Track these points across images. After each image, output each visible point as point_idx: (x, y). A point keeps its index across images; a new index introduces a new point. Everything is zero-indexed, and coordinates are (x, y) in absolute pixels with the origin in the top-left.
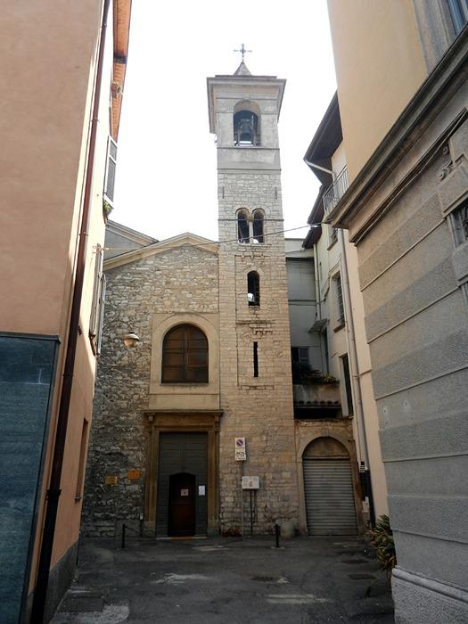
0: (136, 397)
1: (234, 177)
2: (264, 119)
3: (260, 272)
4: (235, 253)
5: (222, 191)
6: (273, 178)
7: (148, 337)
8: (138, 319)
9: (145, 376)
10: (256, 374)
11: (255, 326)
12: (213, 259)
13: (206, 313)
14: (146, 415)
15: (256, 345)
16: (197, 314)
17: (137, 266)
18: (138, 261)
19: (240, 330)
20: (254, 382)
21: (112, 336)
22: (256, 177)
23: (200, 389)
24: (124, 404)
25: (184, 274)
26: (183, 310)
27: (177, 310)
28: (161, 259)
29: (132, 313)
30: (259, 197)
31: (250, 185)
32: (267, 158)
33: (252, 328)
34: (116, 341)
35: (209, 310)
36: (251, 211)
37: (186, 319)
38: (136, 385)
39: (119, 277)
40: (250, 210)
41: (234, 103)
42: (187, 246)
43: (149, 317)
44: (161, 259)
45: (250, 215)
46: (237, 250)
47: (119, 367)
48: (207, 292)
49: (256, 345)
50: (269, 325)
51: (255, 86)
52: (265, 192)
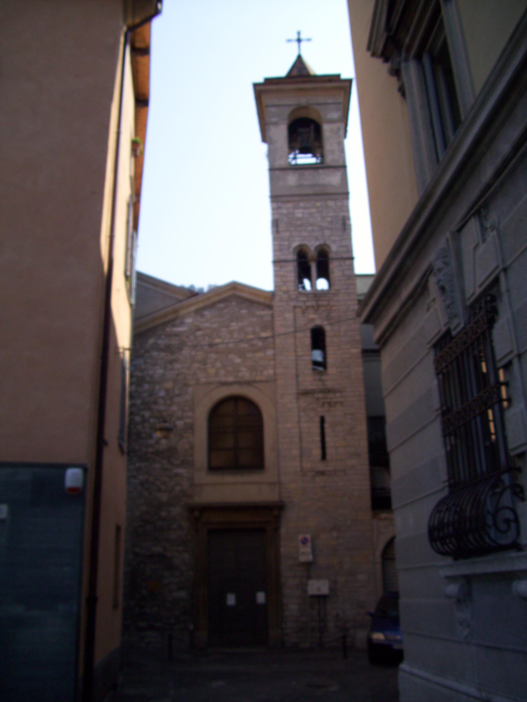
0: (178, 488)
1: (290, 205)
2: (327, 129)
3: (327, 328)
4: (293, 304)
5: (276, 224)
6: (339, 204)
7: (190, 414)
8: (177, 392)
9: (187, 463)
10: (324, 456)
11: (321, 395)
12: (266, 312)
13: (261, 382)
14: (191, 509)
15: (322, 420)
16: (249, 383)
17: (174, 326)
18: (174, 320)
19: (304, 402)
20: (321, 466)
21: (147, 414)
22: (318, 204)
23: (255, 477)
24: (164, 497)
25: (231, 333)
26: (231, 379)
27: (223, 379)
28: (202, 316)
29: (169, 385)
30: (322, 229)
31: (311, 215)
32: (334, 179)
33: (318, 399)
34: (152, 420)
35: (263, 378)
36: (312, 249)
37: (236, 390)
38: (177, 475)
39: (151, 341)
40: (312, 245)
41: (287, 111)
42: (235, 296)
43: (190, 390)
44: (202, 316)
45: (312, 252)
46: (296, 300)
47: (157, 453)
48: (260, 355)
49: (322, 420)
50: (338, 395)
51: (314, 89)
52: (331, 222)
